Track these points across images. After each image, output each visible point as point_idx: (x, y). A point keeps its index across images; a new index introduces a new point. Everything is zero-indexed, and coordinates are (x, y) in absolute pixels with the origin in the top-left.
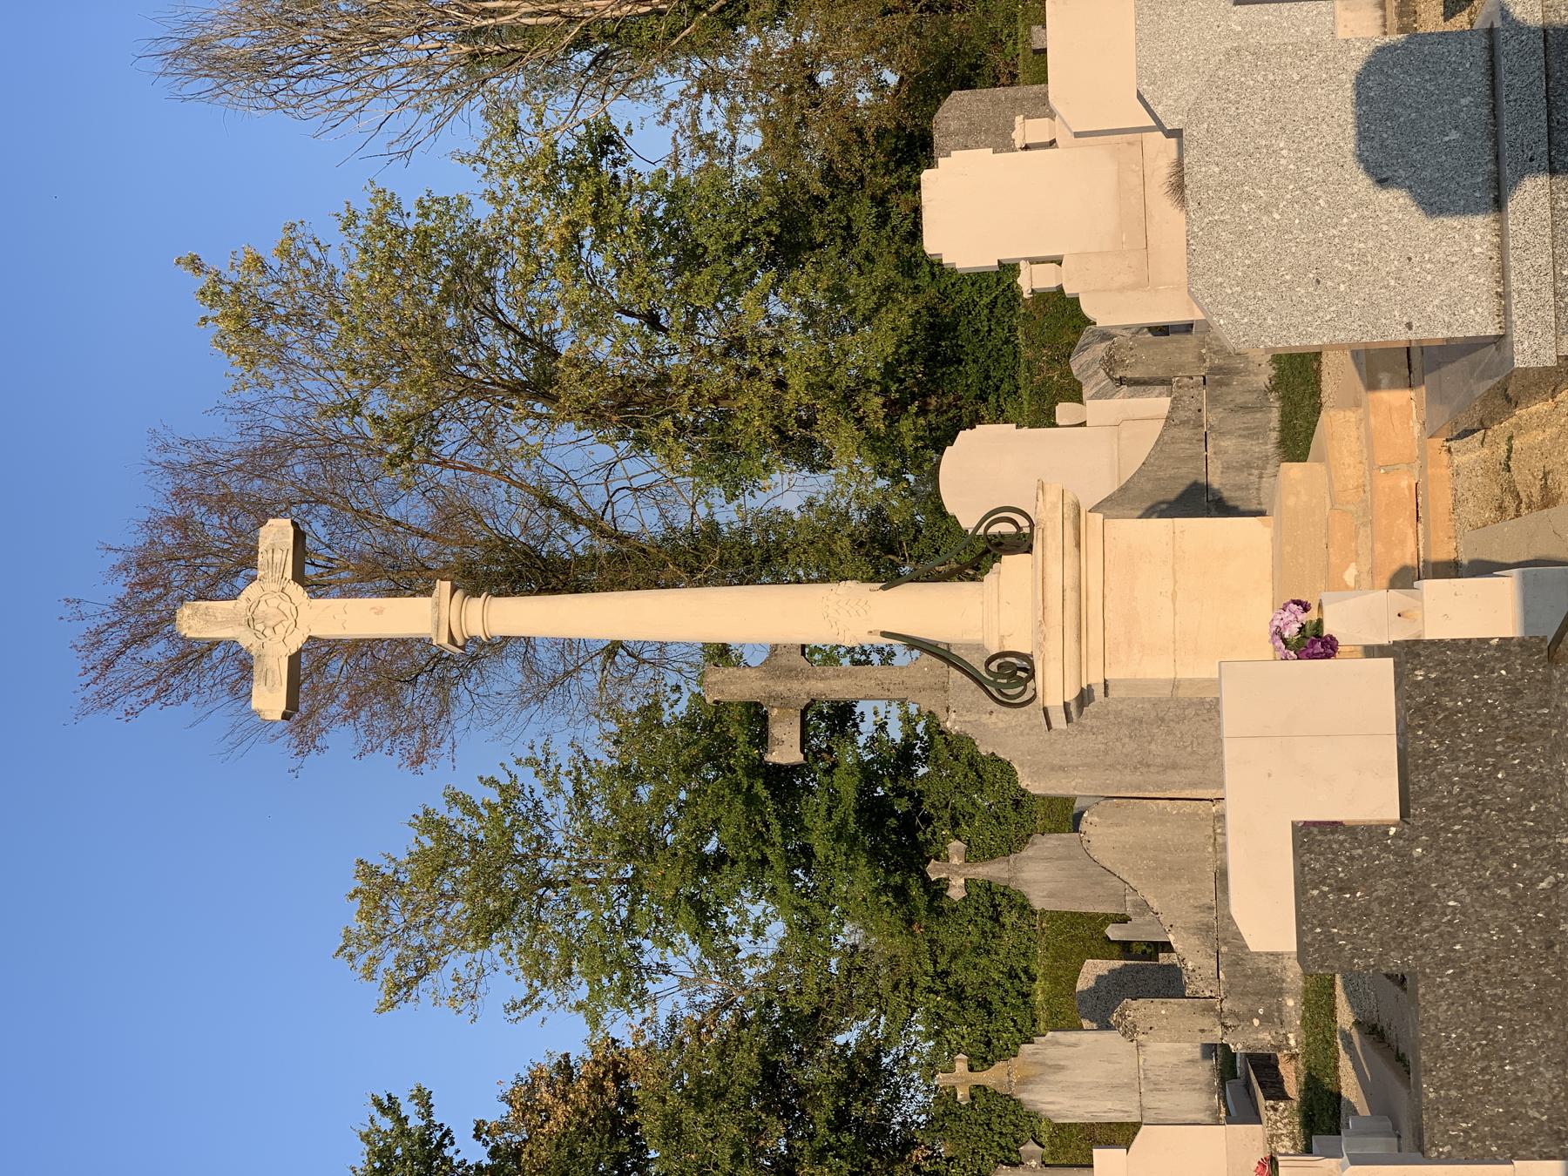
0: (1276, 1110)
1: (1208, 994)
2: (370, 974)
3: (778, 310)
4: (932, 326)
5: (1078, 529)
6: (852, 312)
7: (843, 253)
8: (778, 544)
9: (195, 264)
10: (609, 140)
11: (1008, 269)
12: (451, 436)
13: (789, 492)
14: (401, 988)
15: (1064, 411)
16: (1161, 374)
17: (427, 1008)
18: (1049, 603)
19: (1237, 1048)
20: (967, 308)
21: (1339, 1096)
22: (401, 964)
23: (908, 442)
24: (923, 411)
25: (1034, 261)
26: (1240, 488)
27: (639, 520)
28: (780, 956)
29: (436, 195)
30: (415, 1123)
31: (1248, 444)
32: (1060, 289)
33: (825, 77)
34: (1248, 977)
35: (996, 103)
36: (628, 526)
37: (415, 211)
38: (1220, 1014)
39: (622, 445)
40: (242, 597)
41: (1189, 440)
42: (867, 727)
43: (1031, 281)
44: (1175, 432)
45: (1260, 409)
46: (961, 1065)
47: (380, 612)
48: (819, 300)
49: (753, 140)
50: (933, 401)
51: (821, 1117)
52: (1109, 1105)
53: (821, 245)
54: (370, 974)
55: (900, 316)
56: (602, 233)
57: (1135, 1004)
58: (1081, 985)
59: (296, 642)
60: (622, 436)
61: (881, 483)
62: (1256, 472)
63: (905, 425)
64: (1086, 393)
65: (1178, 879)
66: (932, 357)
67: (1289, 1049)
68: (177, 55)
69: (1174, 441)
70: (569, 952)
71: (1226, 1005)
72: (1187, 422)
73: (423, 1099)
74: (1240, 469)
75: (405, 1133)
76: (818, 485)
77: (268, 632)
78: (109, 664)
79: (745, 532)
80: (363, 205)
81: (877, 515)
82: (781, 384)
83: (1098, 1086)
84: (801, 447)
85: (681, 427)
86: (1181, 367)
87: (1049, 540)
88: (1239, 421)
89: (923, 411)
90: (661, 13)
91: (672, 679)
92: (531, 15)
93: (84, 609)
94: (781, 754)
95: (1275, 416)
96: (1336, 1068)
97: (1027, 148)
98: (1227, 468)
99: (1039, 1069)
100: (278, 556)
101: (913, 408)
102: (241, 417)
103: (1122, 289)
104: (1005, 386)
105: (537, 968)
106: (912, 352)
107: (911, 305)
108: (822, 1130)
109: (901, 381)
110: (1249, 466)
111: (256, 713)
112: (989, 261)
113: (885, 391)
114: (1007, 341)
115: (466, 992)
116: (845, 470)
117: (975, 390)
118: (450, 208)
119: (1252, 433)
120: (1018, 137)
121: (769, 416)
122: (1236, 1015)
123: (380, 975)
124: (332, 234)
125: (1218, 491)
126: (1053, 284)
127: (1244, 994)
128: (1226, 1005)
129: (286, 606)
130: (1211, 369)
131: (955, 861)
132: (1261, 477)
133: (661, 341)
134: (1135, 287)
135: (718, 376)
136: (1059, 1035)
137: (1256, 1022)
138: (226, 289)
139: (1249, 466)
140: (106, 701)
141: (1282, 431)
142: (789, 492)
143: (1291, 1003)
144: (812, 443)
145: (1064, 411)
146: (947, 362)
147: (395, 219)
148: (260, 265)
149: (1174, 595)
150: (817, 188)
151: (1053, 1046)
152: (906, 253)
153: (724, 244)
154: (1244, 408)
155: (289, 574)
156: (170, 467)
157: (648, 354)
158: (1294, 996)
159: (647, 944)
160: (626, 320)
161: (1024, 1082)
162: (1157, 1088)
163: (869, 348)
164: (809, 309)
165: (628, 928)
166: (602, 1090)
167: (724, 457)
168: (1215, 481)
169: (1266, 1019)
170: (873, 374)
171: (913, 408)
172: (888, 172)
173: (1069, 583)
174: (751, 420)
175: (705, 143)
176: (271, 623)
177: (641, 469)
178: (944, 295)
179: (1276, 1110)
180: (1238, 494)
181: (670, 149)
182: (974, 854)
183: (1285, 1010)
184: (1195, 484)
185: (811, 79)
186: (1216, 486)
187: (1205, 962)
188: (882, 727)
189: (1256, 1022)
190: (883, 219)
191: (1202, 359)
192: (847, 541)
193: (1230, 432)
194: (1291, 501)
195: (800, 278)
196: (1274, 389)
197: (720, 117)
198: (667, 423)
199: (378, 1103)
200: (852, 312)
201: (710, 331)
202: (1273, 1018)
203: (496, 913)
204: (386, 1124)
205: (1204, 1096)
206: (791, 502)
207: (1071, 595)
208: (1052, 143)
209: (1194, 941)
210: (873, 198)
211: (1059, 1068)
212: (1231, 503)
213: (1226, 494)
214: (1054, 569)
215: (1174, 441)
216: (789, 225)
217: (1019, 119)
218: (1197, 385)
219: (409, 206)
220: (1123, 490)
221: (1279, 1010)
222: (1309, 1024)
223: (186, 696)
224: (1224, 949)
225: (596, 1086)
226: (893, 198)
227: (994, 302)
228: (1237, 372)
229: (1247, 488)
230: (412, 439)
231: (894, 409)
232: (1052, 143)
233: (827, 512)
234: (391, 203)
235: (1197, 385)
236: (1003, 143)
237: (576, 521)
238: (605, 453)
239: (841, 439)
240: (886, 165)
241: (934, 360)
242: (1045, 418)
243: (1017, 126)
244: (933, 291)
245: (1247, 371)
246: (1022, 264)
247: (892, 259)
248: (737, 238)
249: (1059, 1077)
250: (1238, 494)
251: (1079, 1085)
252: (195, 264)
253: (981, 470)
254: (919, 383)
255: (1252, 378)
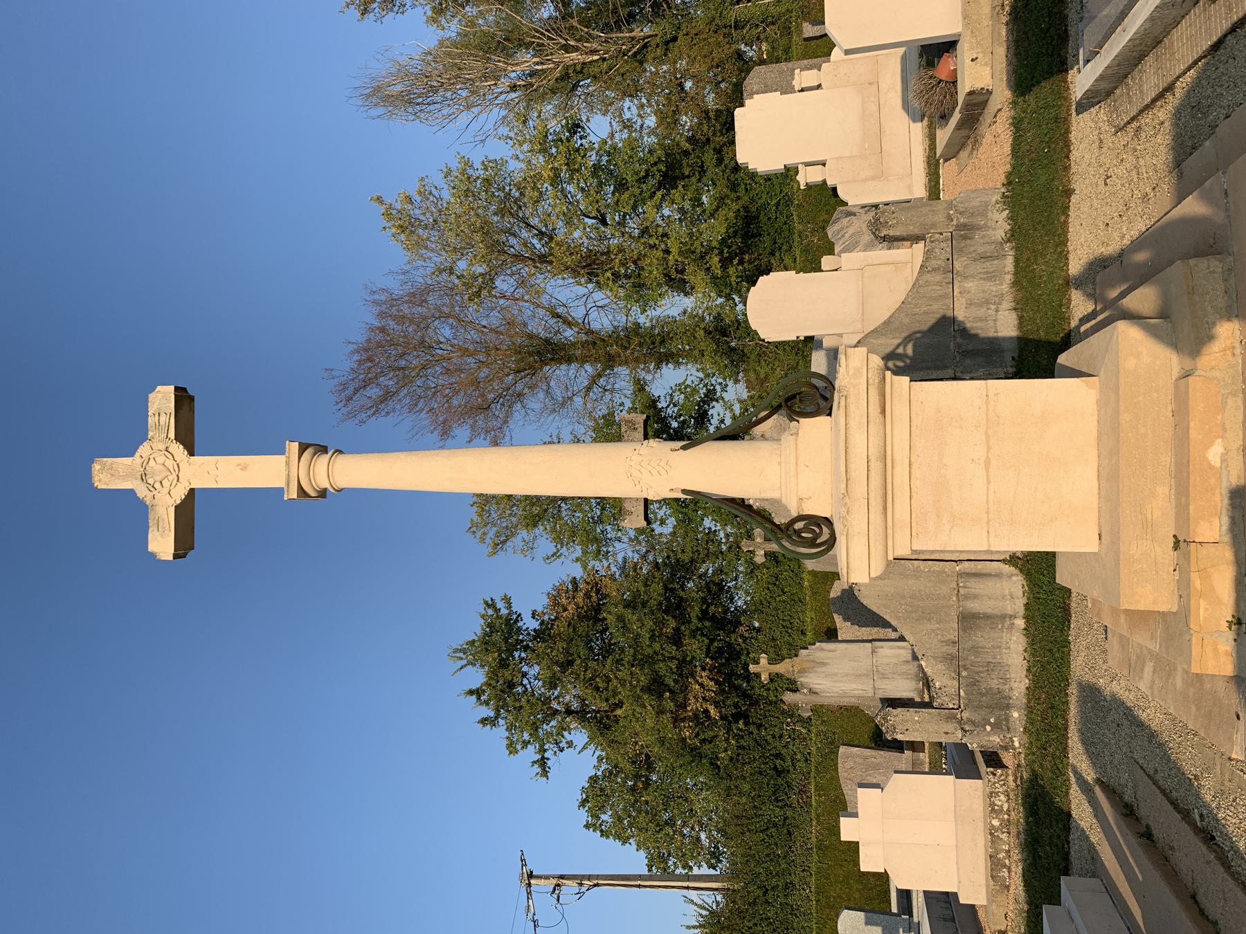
0: (995, 775)
1: (951, 706)
2: (483, 540)
3: (666, 212)
4: (746, 217)
5: (882, 395)
6: (704, 211)
7: (699, 180)
8: (669, 333)
9: (379, 200)
10: (578, 126)
11: (790, 173)
12: (504, 284)
13: (674, 306)
14: (499, 545)
15: (826, 261)
16: (917, 231)
17: (510, 556)
18: (853, 474)
19: (973, 746)
20: (765, 206)
21: (1069, 815)
22: (498, 535)
23: (733, 279)
24: (741, 262)
25: (807, 164)
26: (981, 320)
27: (602, 322)
28: (674, 534)
29: (491, 158)
30: (504, 612)
31: (988, 285)
32: (824, 182)
33: (688, 85)
34: (983, 695)
35: (781, 72)
36: (595, 326)
37: (480, 167)
38: (960, 722)
39: (590, 286)
40: (137, 454)
41: (939, 283)
42: (715, 422)
43: (807, 177)
44: (928, 277)
45: (997, 258)
46: (764, 660)
47: (244, 468)
48: (687, 205)
49: (651, 121)
50: (747, 257)
51: (695, 612)
52: (854, 686)
53: (688, 177)
54: (483, 540)
55: (729, 212)
56: (573, 171)
57: (895, 712)
58: (833, 595)
59: (179, 494)
60: (590, 281)
61: (720, 300)
62: (993, 307)
63: (731, 270)
64: (837, 249)
65: (929, 620)
66: (746, 233)
67: (1014, 749)
68: (368, 96)
69: (927, 284)
70: (573, 534)
71: (966, 715)
72: (938, 269)
73: (507, 600)
74: (980, 305)
75: (499, 617)
76: (688, 302)
77: (157, 485)
78: (349, 399)
79: (653, 327)
80: (455, 165)
81: (718, 318)
82: (667, 252)
83: (847, 675)
84: (679, 284)
85: (616, 276)
86: (933, 225)
87: (852, 408)
88: (979, 267)
89: (741, 262)
90: (604, 59)
91: (617, 400)
92: (537, 64)
93: (334, 373)
94: (630, 521)
95: (1009, 263)
96: (1067, 793)
97: (802, 90)
98: (970, 304)
99: (811, 665)
100: (163, 419)
101: (735, 262)
102: (402, 277)
103: (865, 180)
104: (785, 247)
105: (558, 540)
106: (735, 232)
107: (734, 207)
108: (695, 621)
109: (730, 247)
110: (987, 302)
111: (153, 555)
112: (779, 166)
113: (721, 253)
114: (785, 223)
115: (529, 547)
116: (700, 295)
117: (768, 250)
118: (498, 165)
119: (990, 276)
120: (797, 84)
121: (661, 268)
122: (973, 723)
123: (488, 540)
124: (439, 180)
125: (962, 322)
126: (819, 179)
127: (979, 707)
128: (966, 715)
129: (170, 463)
130: (957, 226)
131: (758, 540)
132: (997, 311)
133: (608, 231)
134: (874, 178)
135: (636, 248)
136: (823, 645)
137: (988, 728)
138: (394, 212)
139: (987, 302)
140: (351, 415)
141: (1015, 274)
142: (674, 306)
143: (1016, 715)
144: (684, 281)
145: (826, 261)
146: (754, 236)
147: (470, 172)
148: (409, 200)
149: (987, 463)
150: (687, 146)
151: (822, 651)
152: (732, 178)
153: (636, 177)
154: (984, 257)
155: (172, 435)
156: (375, 302)
157: (601, 238)
158: (1019, 709)
159: (609, 528)
160: (586, 220)
161: (802, 671)
162: (884, 677)
163: (714, 230)
164: (682, 210)
165: (600, 520)
166: (590, 597)
167: (639, 290)
168: (960, 314)
169: (996, 727)
170: (715, 244)
171: (735, 262)
172: (722, 134)
173: (874, 452)
174: (653, 271)
175: (627, 125)
176: (159, 478)
177: (600, 297)
178: (752, 200)
179: (995, 775)
180: (979, 324)
181: (608, 129)
182: (772, 662)
183: (1012, 720)
184: (944, 317)
185: (681, 85)
186: (960, 318)
187: (949, 683)
188: (722, 421)
189: (988, 728)
190: (720, 161)
191: (950, 218)
192: (702, 332)
193: (973, 276)
194: (1131, 364)
195: (676, 194)
196: (1009, 241)
197: (635, 111)
198: (608, 274)
199: (486, 603)
200: (704, 211)
201: (633, 226)
202: (1002, 725)
203: (537, 515)
204: (490, 612)
205: (914, 683)
206: (674, 312)
207: (876, 466)
208: (819, 87)
209: (941, 666)
210: (714, 150)
211: (823, 664)
212: (973, 332)
213: (968, 325)
214: (859, 441)
215: (927, 284)
216: (670, 167)
217: (797, 71)
218: (945, 240)
219: (478, 165)
220: (887, 323)
221: (1007, 720)
222: (1031, 728)
223: (388, 413)
224: (964, 674)
225: (587, 595)
226: (725, 149)
227: (778, 203)
228: (979, 228)
229: (986, 320)
230: (481, 288)
231: (725, 262)
232: (819, 87)
233: (692, 316)
234: (468, 163)
235: (945, 240)
236: (787, 89)
237: (570, 324)
238: (581, 290)
239: (696, 277)
240: (721, 131)
241: (747, 236)
242: (814, 266)
243: (796, 76)
244: (746, 198)
245: (986, 227)
246: (800, 167)
247: (725, 182)
248: (643, 174)
249: (824, 669)
250: (979, 324)
251: (836, 674)
252: (379, 200)
253: (778, 306)
254: (739, 248)
255: (991, 232)
